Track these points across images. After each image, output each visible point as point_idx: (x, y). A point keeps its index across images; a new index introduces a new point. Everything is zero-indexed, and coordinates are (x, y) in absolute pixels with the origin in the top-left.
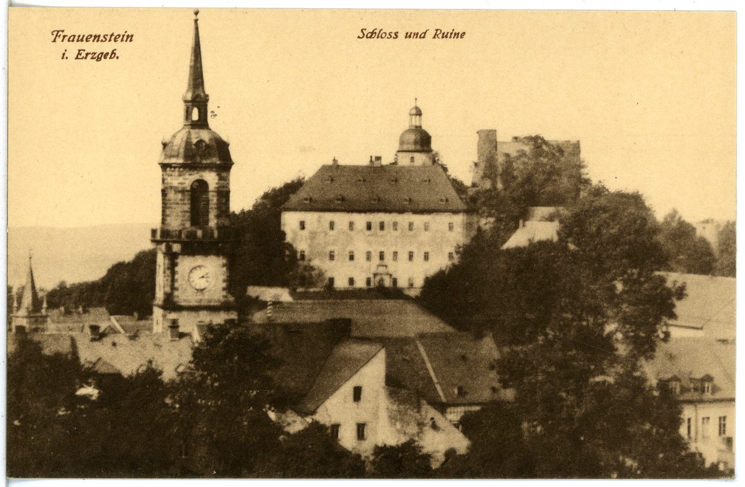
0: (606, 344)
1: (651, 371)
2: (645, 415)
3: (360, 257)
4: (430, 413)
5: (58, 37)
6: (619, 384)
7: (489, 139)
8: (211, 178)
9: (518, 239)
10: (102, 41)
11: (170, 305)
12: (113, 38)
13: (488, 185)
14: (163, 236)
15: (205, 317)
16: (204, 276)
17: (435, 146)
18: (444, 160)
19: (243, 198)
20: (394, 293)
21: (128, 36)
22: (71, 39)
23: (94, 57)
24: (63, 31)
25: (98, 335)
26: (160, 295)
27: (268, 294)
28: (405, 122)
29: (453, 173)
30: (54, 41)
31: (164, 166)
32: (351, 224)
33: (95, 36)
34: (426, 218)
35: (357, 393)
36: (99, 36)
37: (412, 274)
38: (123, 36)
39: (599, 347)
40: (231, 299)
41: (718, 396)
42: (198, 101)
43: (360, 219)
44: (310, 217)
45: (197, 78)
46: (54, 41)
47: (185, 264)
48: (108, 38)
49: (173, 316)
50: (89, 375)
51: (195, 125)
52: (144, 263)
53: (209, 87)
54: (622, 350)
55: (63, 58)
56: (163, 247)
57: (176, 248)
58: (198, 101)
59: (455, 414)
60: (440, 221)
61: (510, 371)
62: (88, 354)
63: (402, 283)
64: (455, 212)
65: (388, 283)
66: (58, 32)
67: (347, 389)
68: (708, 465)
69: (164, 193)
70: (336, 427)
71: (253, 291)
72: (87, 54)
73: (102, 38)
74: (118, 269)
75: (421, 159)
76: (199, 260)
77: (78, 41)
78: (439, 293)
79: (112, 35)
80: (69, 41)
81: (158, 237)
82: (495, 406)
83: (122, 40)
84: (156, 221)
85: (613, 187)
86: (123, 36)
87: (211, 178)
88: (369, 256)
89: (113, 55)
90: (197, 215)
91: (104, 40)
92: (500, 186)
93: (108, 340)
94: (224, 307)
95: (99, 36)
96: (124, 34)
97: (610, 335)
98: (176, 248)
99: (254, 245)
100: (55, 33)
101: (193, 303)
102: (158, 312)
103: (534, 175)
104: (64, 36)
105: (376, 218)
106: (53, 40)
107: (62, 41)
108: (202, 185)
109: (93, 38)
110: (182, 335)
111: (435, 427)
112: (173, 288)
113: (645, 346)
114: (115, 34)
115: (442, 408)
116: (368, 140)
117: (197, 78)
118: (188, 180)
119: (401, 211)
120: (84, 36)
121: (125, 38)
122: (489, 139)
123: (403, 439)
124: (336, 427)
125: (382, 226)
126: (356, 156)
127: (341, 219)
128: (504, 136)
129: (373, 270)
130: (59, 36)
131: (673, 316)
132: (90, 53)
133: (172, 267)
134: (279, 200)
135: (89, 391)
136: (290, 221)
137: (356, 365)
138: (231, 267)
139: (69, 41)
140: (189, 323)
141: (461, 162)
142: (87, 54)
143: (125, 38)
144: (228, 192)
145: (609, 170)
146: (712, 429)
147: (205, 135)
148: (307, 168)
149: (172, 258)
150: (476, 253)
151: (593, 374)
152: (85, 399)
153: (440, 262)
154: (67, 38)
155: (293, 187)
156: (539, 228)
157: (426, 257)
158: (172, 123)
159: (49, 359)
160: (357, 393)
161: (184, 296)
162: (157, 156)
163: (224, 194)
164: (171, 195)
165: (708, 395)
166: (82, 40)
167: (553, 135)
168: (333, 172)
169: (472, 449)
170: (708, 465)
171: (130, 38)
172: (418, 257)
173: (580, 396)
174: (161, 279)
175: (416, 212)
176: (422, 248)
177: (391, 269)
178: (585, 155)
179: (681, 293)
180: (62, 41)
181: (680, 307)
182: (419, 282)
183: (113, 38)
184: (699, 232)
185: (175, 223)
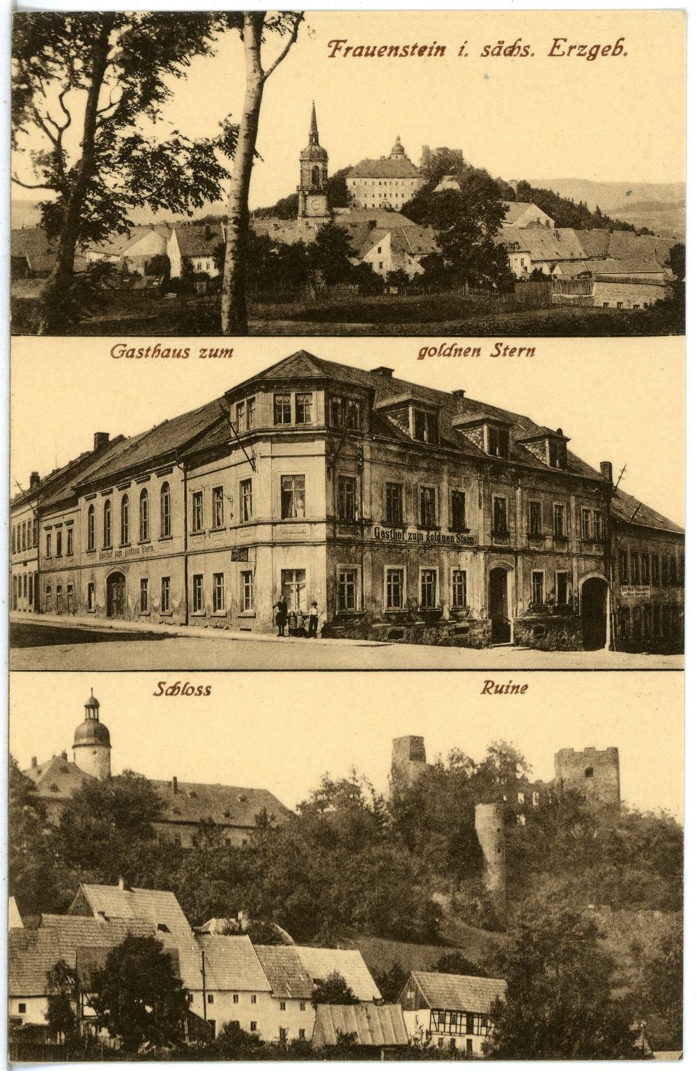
0: (479, 231)
1: (497, 241)
2: (494, 258)
3: (377, 196)
4: (408, 257)
6: (484, 246)
8: (320, 165)
9: (439, 188)
10: (401, 55)
11: (305, 216)
14: (301, 188)
16: (317, 204)
17: (406, 152)
18: (409, 157)
19: (332, 171)
20: (391, 210)
21: (438, 48)
22: (357, 52)
24: (345, 41)
25: (277, 228)
26: (300, 212)
27: (341, 210)
28: (393, 143)
29: (413, 162)
30: (333, 56)
31: (301, 161)
32: (373, 183)
33: (392, 48)
34: (402, 180)
36: (397, 48)
37: (397, 202)
39: (475, 231)
40: (328, 213)
41: (520, 250)
42: (314, 136)
43: (377, 181)
44: (357, 180)
46: (333, 56)
47: (310, 199)
48: (410, 50)
49: (305, 220)
50: (275, 244)
51: (314, 144)
52: (294, 199)
53: (319, 129)
54: (484, 232)
57: (307, 193)
58: (314, 136)
59: (418, 258)
60: (408, 181)
61: (440, 240)
62: (273, 235)
63: (393, 206)
65: (388, 206)
66: (338, 42)
67: (375, 249)
68: (518, 278)
69: (301, 171)
70: (371, 264)
71: (335, 210)
72: (571, 48)
73: (400, 51)
75: (400, 157)
77: (367, 55)
78: (407, 210)
79: (415, 47)
80: (354, 55)
82: (434, 255)
83: (430, 54)
84: (298, 183)
85: (476, 166)
87: (320, 165)
88: (380, 196)
90: (315, 180)
91: (404, 54)
93: (281, 230)
94: (326, 216)
95: (397, 48)
97: (480, 227)
98: (307, 193)
99: (336, 191)
100: (334, 45)
102: (299, 218)
103: (445, 163)
105: (383, 181)
106: (330, 54)
107: (345, 55)
108: (317, 167)
109: (388, 50)
111: (410, 263)
113: (493, 230)
114: (420, 46)
115: (412, 255)
116: (380, 150)
118: (311, 166)
119: (393, 178)
120: (375, 48)
121: (434, 51)
123: (398, 268)
124: (371, 264)
126: (376, 157)
127: (370, 181)
130: (340, 49)
131: (504, 218)
132: (575, 47)
134: (343, 175)
135: (275, 250)
136: (349, 182)
138: (328, 200)
139: (354, 55)
140: (312, 222)
143: (434, 51)
144: (327, 171)
145: (475, 159)
149: (305, 197)
150: (426, 191)
151: (473, 241)
152: (274, 253)
153: (408, 198)
154: (351, 52)
157: (403, 196)
158: (304, 143)
159: (259, 238)
161: (310, 212)
162: (298, 156)
163: (325, 171)
164: (304, 172)
165: (516, 250)
166: (372, 54)
167: (451, 147)
168: (366, 163)
169: (426, 273)
170: (518, 278)
173: (468, 250)
174: (301, 206)
176: (402, 191)
177: (389, 201)
179: (507, 209)
180: (345, 55)
181: (507, 215)
182: (400, 206)
183: (416, 51)
185: (306, 183)
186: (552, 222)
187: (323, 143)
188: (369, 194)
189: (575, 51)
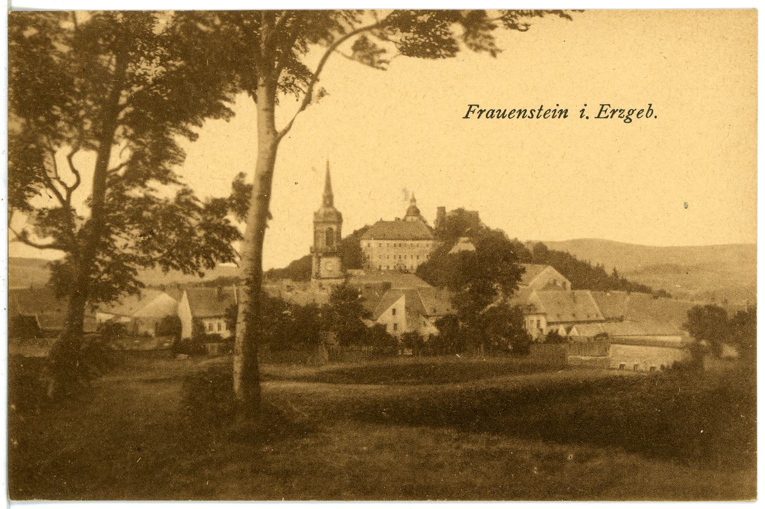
1: (512, 302)
5: (471, 113)
7: (442, 210)
11: (318, 276)
12: (542, 113)
13: (442, 229)
14: (314, 250)
15: (333, 281)
16: (330, 266)
23: (622, 115)
30: (467, 117)
35: (394, 311)
38: (555, 110)
42: (329, 199)
43: (392, 242)
45: (328, 187)
47: (324, 261)
48: (535, 114)
55: (581, 117)
56: (315, 254)
58: (329, 199)
64: (429, 239)
65: (403, 268)
67: (389, 311)
74: (295, 263)
76: (330, 259)
81: (313, 250)
86: (555, 110)
87: (334, 227)
89: (650, 112)
90: (329, 241)
92: (446, 229)
96: (555, 107)
99: (350, 253)
101: (327, 276)
102: (313, 280)
103: (457, 224)
104: (481, 111)
107: (505, 110)
108: (331, 229)
110: (324, 289)
112: (319, 271)
116: (395, 211)
117: (328, 187)
118: (325, 228)
121: (557, 114)
122: (442, 210)
123: (412, 330)
124: (385, 326)
125: (400, 245)
128: (448, 210)
129: (397, 262)
130: (473, 112)
133: (319, 262)
134: (358, 234)
136: (364, 244)
137: (393, 301)
141: (431, 218)
142: (614, 112)
145: (491, 221)
146: (535, 326)
147: (331, 210)
148: (371, 222)
153: (424, 259)
154: (484, 114)
155: (365, 229)
156: (464, 245)
158: (316, 203)
160: (394, 311)
161: (323, 273)
163: (339, 233)
168: (381, 223)
171: (479, 118)
172: (415, 258)
175: (413, 240)
176: (416, 254)
178: (481, 216)
180: (505, 110)
184: (526, 247)
186: (569, 284)
187: (338, 205)
188: (379, 253)
189: (618, 113)
